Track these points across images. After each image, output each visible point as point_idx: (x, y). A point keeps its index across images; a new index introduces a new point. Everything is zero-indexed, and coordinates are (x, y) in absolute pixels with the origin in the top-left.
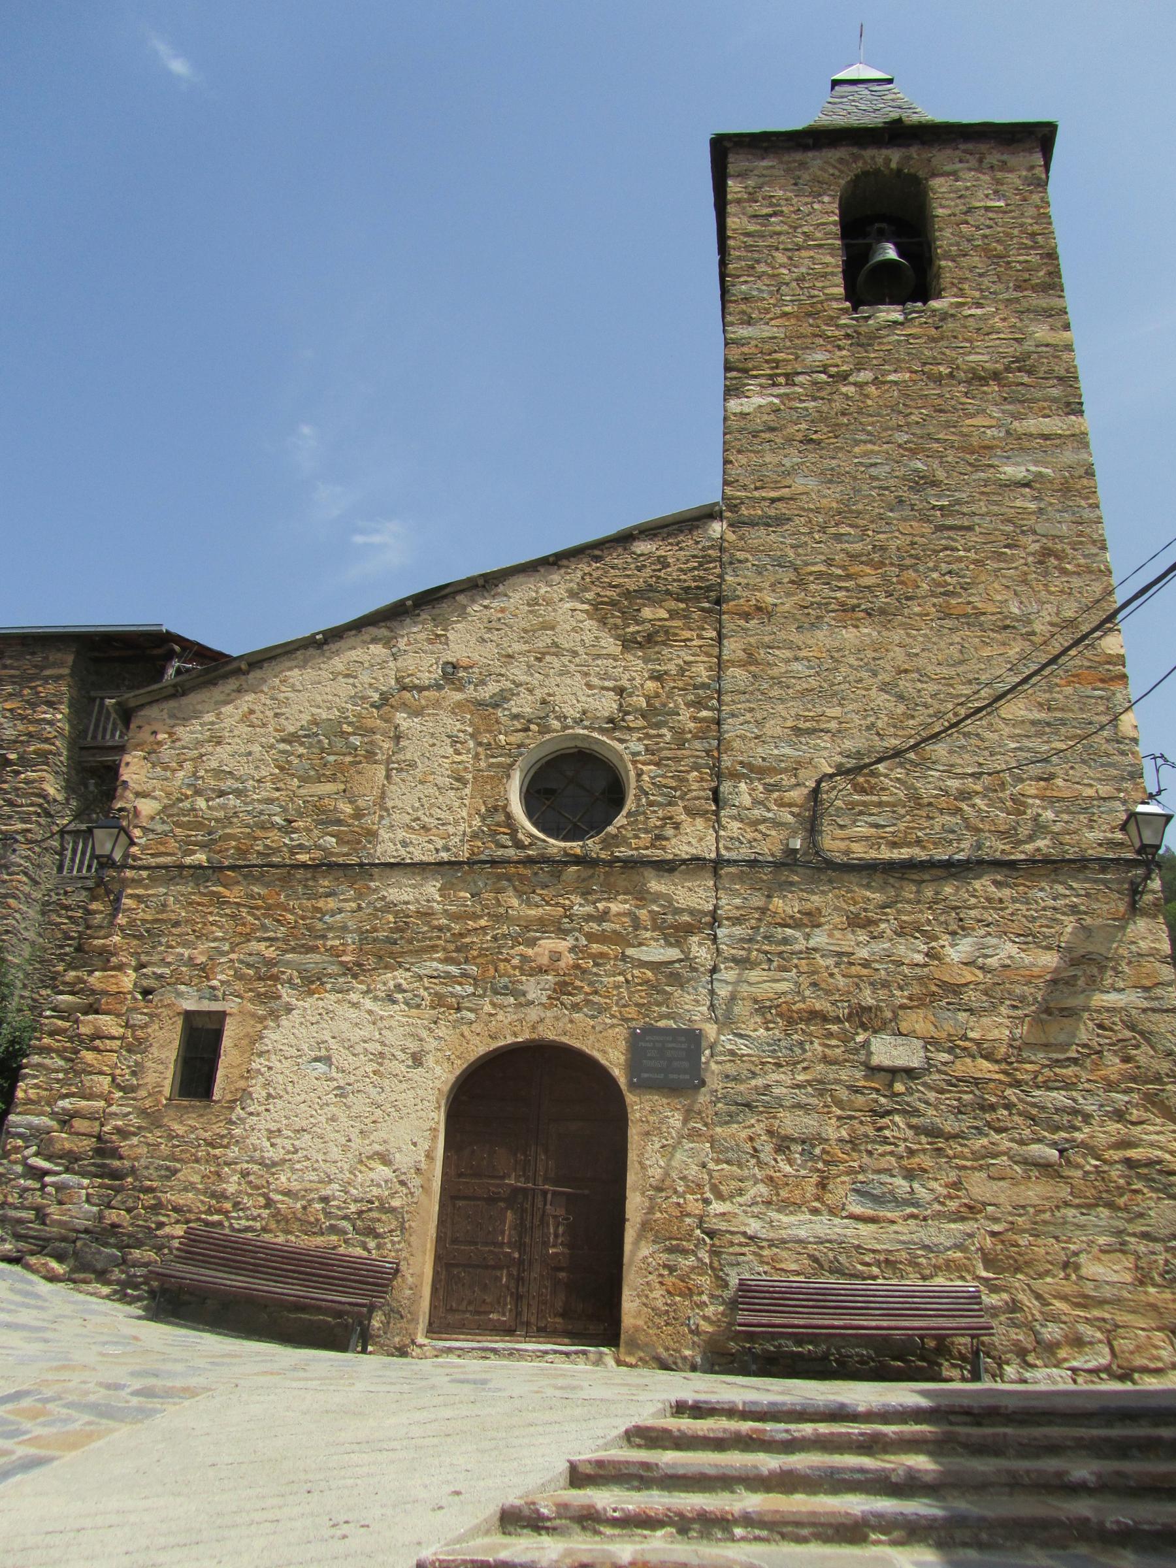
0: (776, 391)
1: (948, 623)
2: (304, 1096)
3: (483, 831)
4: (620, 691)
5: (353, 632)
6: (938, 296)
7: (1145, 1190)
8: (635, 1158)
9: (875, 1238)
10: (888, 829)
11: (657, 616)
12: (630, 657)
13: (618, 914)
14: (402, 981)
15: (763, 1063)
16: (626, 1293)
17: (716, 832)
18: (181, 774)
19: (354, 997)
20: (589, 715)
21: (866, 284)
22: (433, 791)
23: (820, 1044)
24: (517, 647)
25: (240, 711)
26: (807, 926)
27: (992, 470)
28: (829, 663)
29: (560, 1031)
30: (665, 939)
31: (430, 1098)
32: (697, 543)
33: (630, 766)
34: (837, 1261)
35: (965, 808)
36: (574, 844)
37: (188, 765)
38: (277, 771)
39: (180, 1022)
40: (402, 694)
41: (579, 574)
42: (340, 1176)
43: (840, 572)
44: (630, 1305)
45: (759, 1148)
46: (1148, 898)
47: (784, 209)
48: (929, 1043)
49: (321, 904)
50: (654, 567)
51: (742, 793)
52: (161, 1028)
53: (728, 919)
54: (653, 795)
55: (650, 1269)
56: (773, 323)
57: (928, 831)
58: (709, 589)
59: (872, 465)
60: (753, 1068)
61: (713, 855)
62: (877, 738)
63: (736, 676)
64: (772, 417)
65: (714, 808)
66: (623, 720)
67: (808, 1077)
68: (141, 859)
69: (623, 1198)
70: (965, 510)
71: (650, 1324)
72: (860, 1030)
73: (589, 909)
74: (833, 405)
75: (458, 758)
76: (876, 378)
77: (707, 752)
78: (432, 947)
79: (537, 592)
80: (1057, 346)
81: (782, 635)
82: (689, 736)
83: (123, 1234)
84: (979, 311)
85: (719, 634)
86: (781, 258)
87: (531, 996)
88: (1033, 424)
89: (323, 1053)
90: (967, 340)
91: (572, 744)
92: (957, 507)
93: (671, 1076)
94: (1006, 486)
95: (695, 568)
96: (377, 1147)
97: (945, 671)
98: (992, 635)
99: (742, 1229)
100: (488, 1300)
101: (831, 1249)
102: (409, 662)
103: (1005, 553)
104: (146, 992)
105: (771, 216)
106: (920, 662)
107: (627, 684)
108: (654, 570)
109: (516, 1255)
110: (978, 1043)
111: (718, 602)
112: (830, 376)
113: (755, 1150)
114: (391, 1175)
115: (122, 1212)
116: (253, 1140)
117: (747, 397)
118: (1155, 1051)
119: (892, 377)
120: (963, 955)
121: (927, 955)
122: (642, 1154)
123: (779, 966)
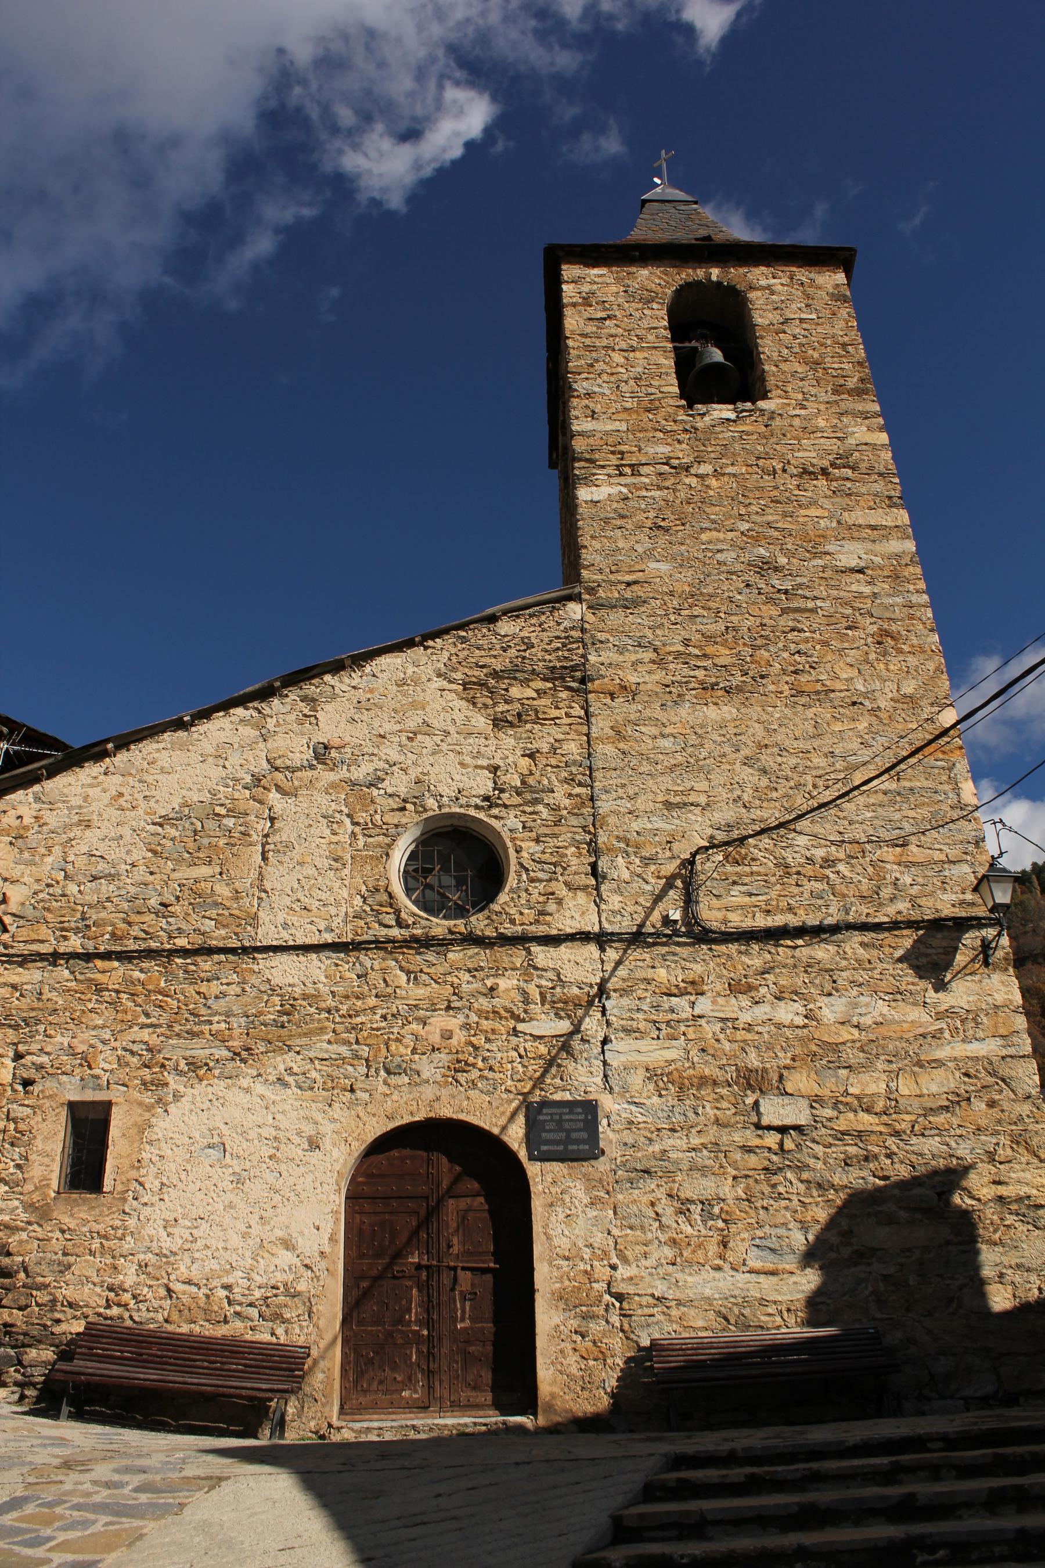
0: (623, 480)
1: (803, 700)
2: (198, 1184)
3: (364, 911)
4: (495, 769)
5: (221, 714)
6: (764, 397)
7: (1017, 1224)
8: (540, 1229)
9: (776, 1290)
10: (760, 898)
11: (526, 695)
12: (501, 735)
13: (507, 990)
14: (293, 1065)
15: (658, 1130)
16: (540, 1361)
17: (598, 906)
18: (49, 860)
19: (245, 1082)
20: (464, 793)
21: (698, 385)
22: (311, 871)
23: (712, 1108)
24: (388, 727)
25: (108, 794)
26: (691, 994)
27: (828, 557)
28: (693, 739)
29: (456, 1108)
30: (556, 1014)
31: (330, 1181)
32: (559, 624)
33: (509, 844)
34: (743, 1315)
35: (831, 876)
36: (458, 922)
37: (57, 850)
38: (150, 854)
39: (64, 1112)
40: (274, 777)
41: (446, 654)
42: (242, 1263)
43: (697, 652)
44: (545, 1373)
45: (660, 1211)
46: (1000, 954)
47: (617, 313)
48: (814, 1101)
49: (203, 988)
50: (518, 648)
51: (618, 868)
52: (44, 1120)
53: (615, 991)
54: (533, 871)
55: (562, 1337)
56: (614, 417)
57: (798, 898)
58: (574, 669)
59: (719, 551)
60: (649, 1135)
61: (596, 929)
62: (744, 811)
63: (605, 751)
64: (621, 505)
65: (594, 882)
66: (499, 798)
67: (702, 1141)
68: (12, 947)
69: (531, 1270)
70: (808, 594)
71: (566, 1390)
72: (749, 1092)
73: (477, 985)
74: (678, 494)
75: (335, 839)
76: (716, 470)
77: (584, 827)
78: (321, 1029)
79: (405, 673)
80: (875, 444)
81: (647, 713)
82: (565, 812)
83: (18, 1334)
84: (803, 412)
85: (587, 712)
86: (618, 358)
87: (425, 1075)
88: (859, 516)
89: (216, 1140)
90: (795, 438)
91: (449, 822)
92: (800, 592)
93: (570, 1147)
94: (842, 572)
95: (558, 649)
96: (279, 1233)
97: (801, 745)
98: (841, 710)
99: (650, 1291)
100: (399, 1378)
101: (736, 1304)
102: (279, 743)
103: (847, 635)
104: (27, 1083)
105: (605, 319)
106: (779, 738)
107: (498, 761)
108: (519, 651)
109: (425, 1332)
110: (858, 1098)
111: (583, 681)
112: (672, 467)
113: (657, 1214)
114: (296, 1261)
115: (14, 1311)
116: (149, 1230)
117: (597, 486)
118: (1016, 1095)
119: (730, 470)
120: (838, 1015)
121: (806, 1017)
122: (547, 1225)
123: (667, 1034)
